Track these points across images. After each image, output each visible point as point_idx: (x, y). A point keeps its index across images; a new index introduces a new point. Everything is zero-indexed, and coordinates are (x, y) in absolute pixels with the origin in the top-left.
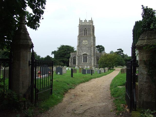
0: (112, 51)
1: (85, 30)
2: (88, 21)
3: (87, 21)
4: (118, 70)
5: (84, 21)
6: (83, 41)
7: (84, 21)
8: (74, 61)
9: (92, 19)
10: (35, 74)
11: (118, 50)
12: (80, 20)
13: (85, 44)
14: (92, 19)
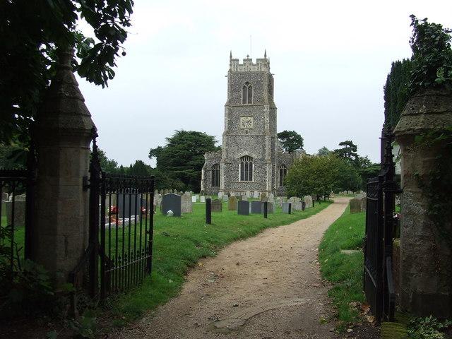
0: (325, 149)
1: (247, 88)
2: (254, 62)
3: (251, 60)
4: (343, 204)
5: (244, 60)
6: (242, 119)
7: (244, 60)
8: (213, 178)
9: (265, 56)
10: (100, 215)
11: (341, 144)
12: (231, 57)
13: (247, 126)
14: (265, 56)
